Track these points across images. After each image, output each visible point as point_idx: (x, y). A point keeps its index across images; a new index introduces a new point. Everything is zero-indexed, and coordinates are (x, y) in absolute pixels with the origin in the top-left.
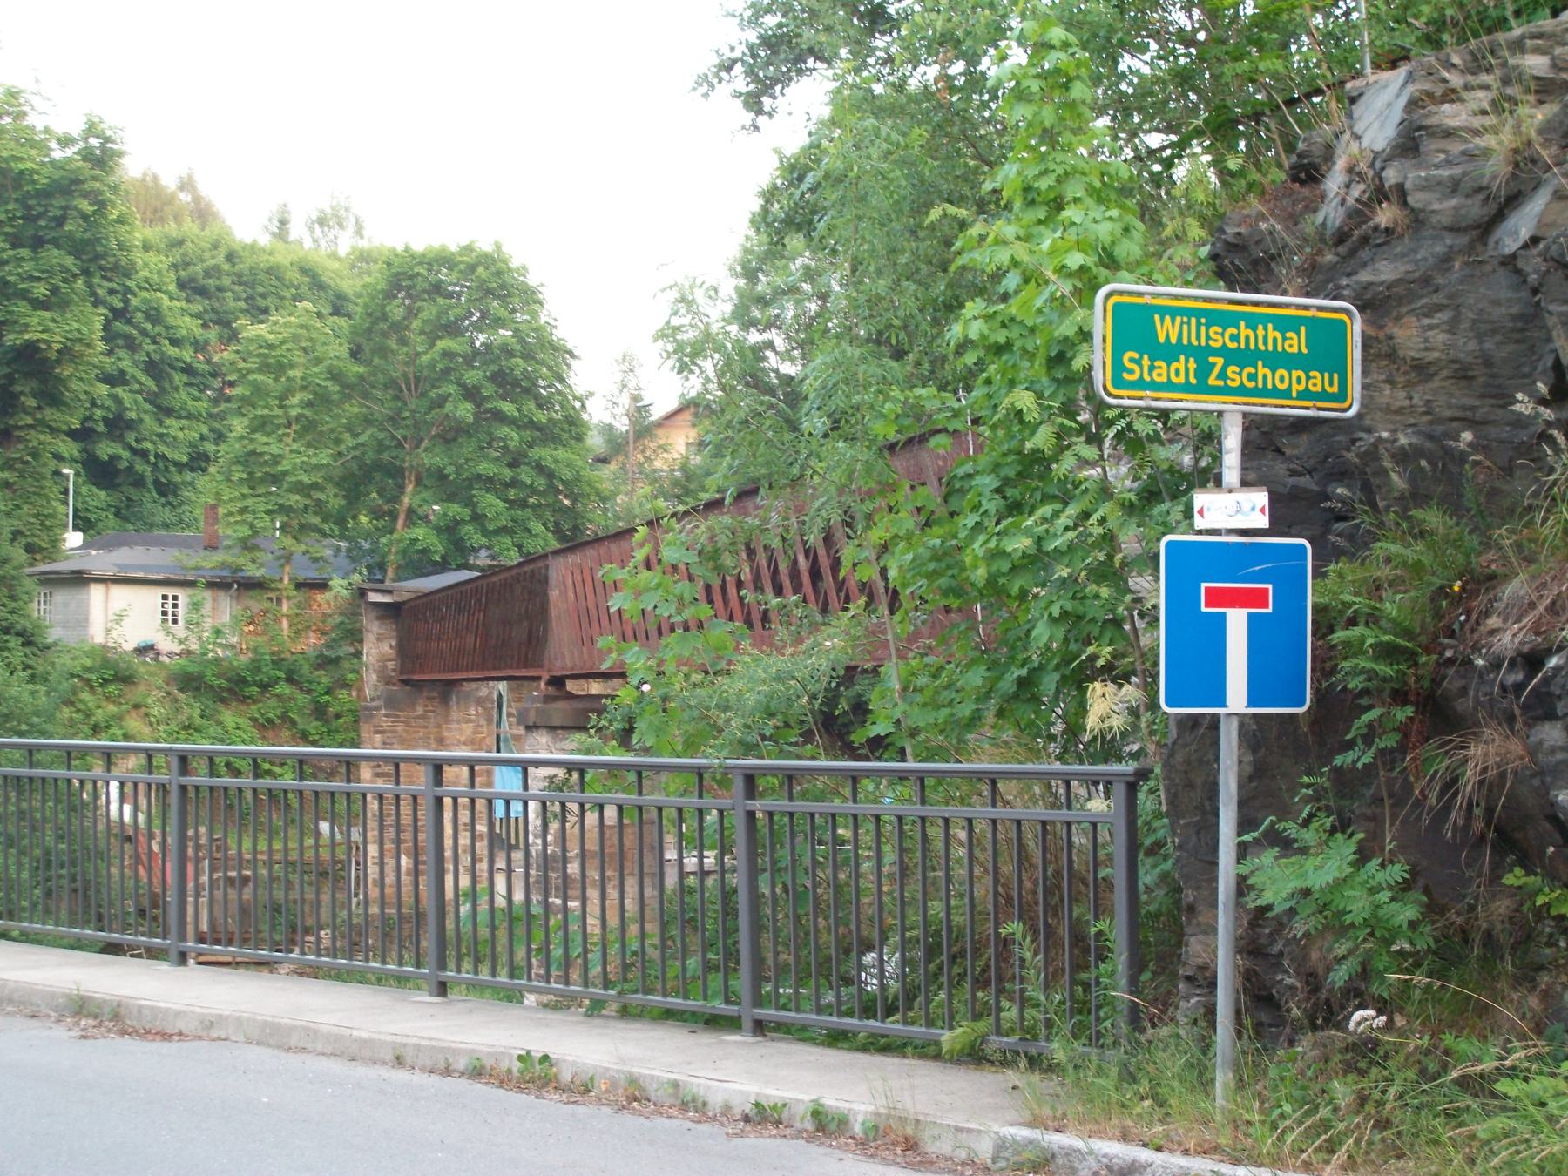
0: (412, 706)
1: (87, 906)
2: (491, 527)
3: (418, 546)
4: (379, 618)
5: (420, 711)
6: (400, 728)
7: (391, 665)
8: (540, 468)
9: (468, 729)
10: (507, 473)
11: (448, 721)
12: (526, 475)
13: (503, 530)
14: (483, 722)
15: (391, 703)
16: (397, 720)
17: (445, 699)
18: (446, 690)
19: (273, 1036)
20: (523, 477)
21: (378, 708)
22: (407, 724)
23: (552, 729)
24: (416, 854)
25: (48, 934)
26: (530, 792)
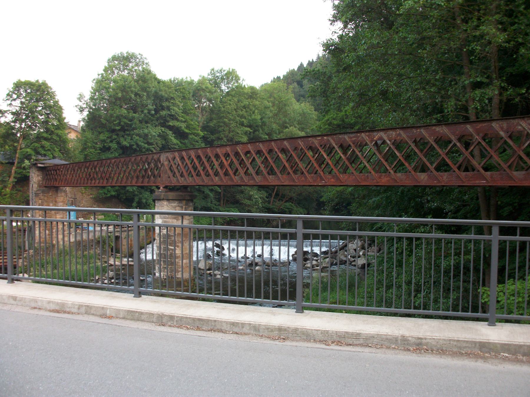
0: (49, 193)
1: (466, 298)
2: (46, 149)
3: (29, 153)
4: (38, 171)
5: (50, 194)
6: (46, 198)
7: (41, 182)
8: (57, 135)
9: (62, 198)
10: (50, 137)
11: (58, 197)
12: (55, 137)
13: (49, 150)
14: (65, 197)
15: (43, 192)
16: (45, 196)
17: (57, 191)
18: (56, 189)
19: (88, 310)
20: (53, 137)
21: (40, 193)
22: (47, 197)
23: (168, 200)
24: (438, 266)
25: (239, 286)
26: (71, 219)
